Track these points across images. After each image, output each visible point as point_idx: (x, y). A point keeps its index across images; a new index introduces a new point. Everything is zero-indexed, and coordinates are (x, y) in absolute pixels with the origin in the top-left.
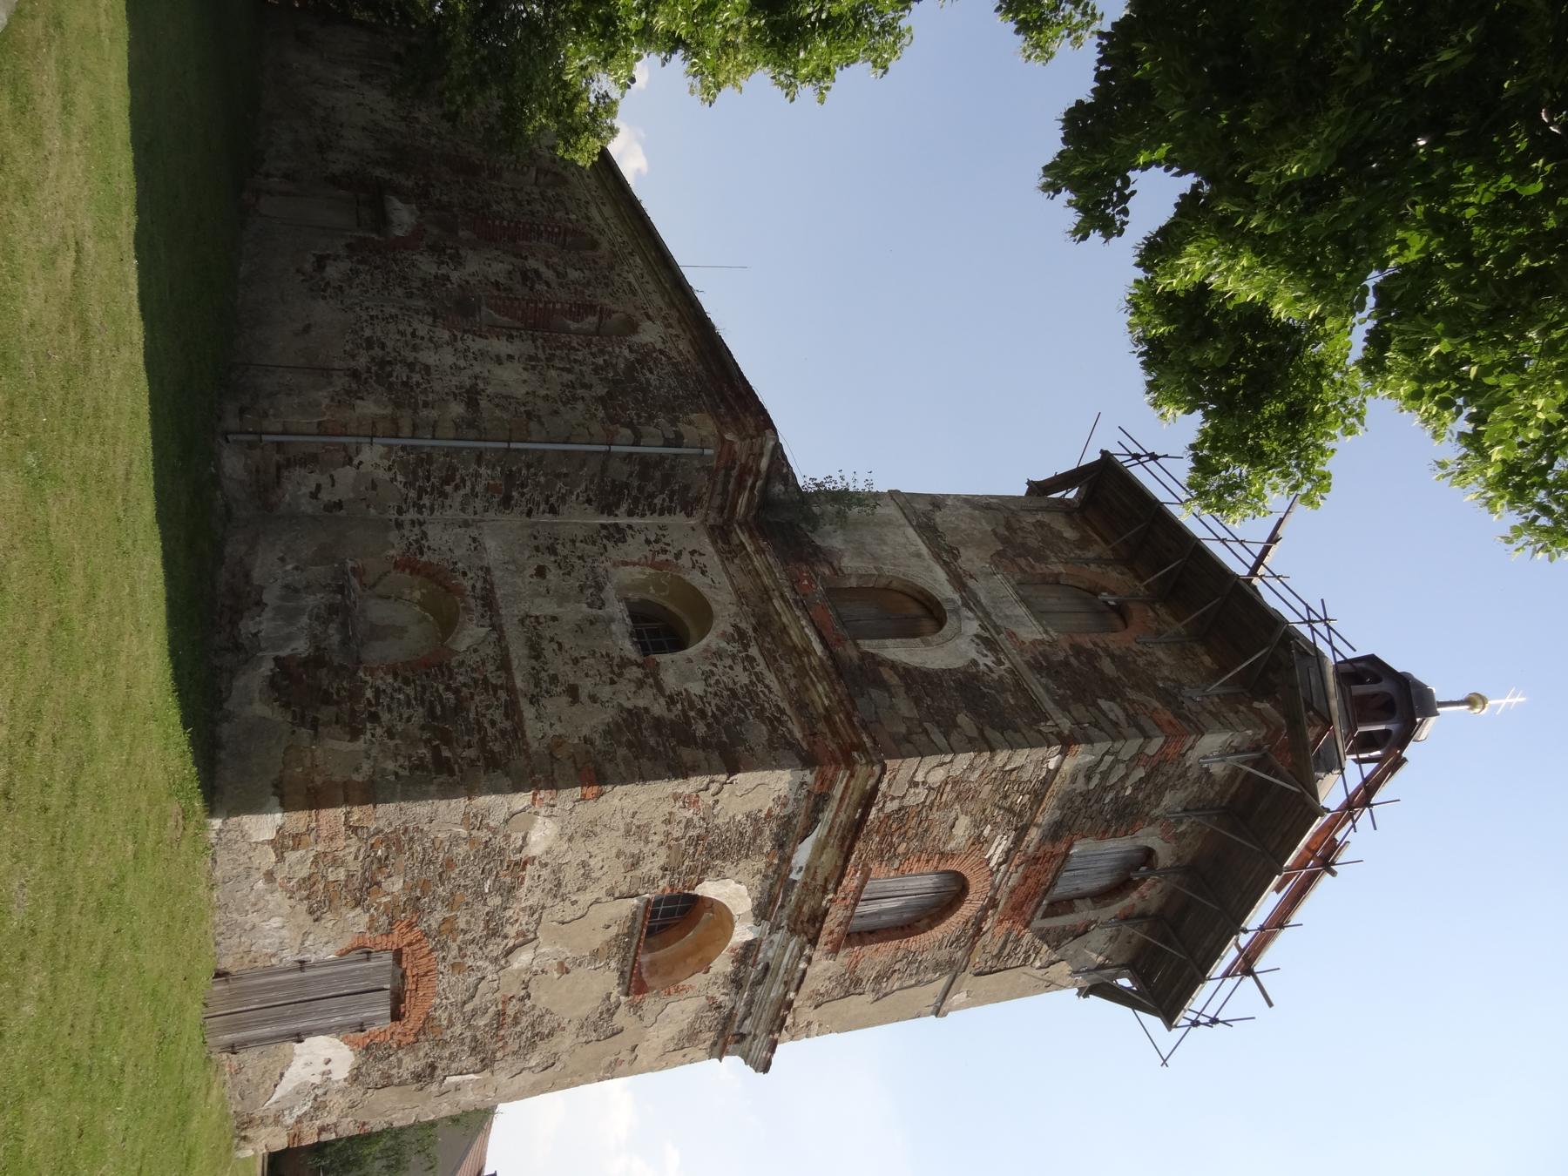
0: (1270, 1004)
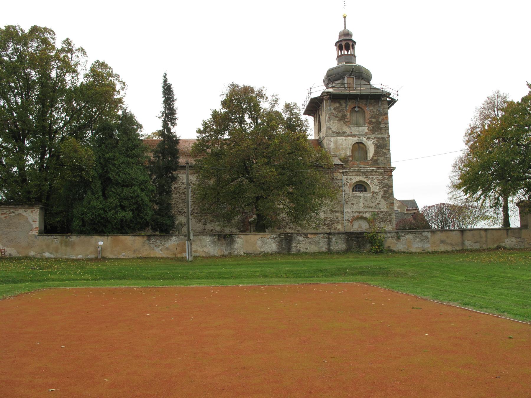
0: (168, 91)
